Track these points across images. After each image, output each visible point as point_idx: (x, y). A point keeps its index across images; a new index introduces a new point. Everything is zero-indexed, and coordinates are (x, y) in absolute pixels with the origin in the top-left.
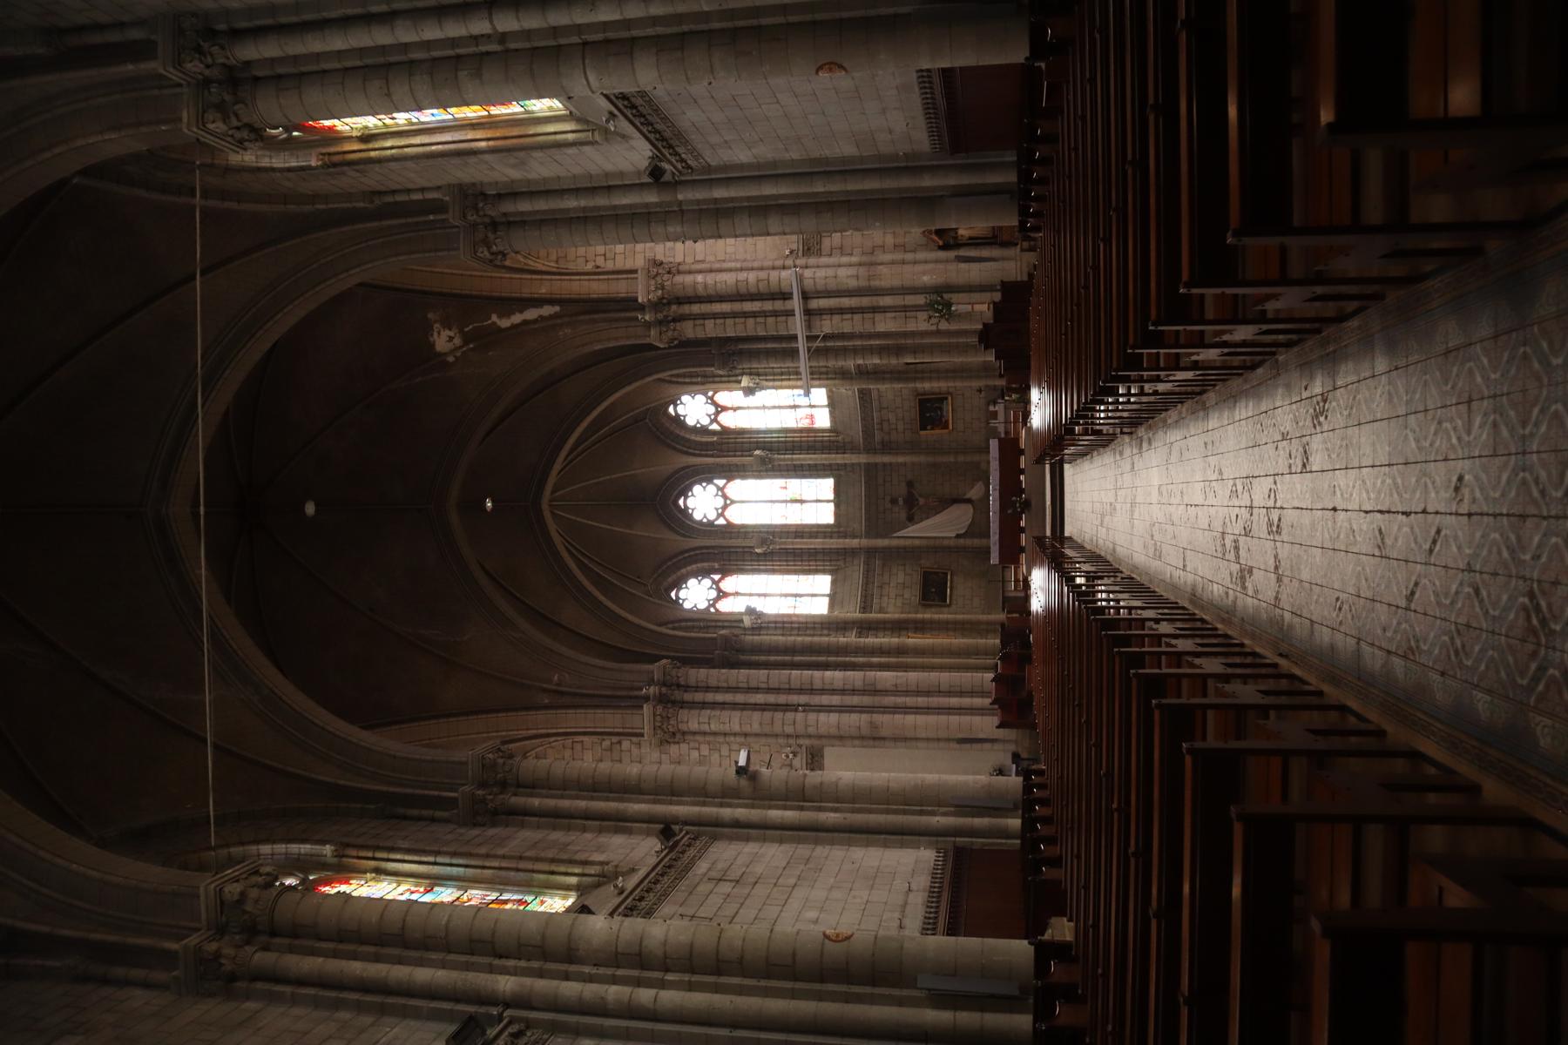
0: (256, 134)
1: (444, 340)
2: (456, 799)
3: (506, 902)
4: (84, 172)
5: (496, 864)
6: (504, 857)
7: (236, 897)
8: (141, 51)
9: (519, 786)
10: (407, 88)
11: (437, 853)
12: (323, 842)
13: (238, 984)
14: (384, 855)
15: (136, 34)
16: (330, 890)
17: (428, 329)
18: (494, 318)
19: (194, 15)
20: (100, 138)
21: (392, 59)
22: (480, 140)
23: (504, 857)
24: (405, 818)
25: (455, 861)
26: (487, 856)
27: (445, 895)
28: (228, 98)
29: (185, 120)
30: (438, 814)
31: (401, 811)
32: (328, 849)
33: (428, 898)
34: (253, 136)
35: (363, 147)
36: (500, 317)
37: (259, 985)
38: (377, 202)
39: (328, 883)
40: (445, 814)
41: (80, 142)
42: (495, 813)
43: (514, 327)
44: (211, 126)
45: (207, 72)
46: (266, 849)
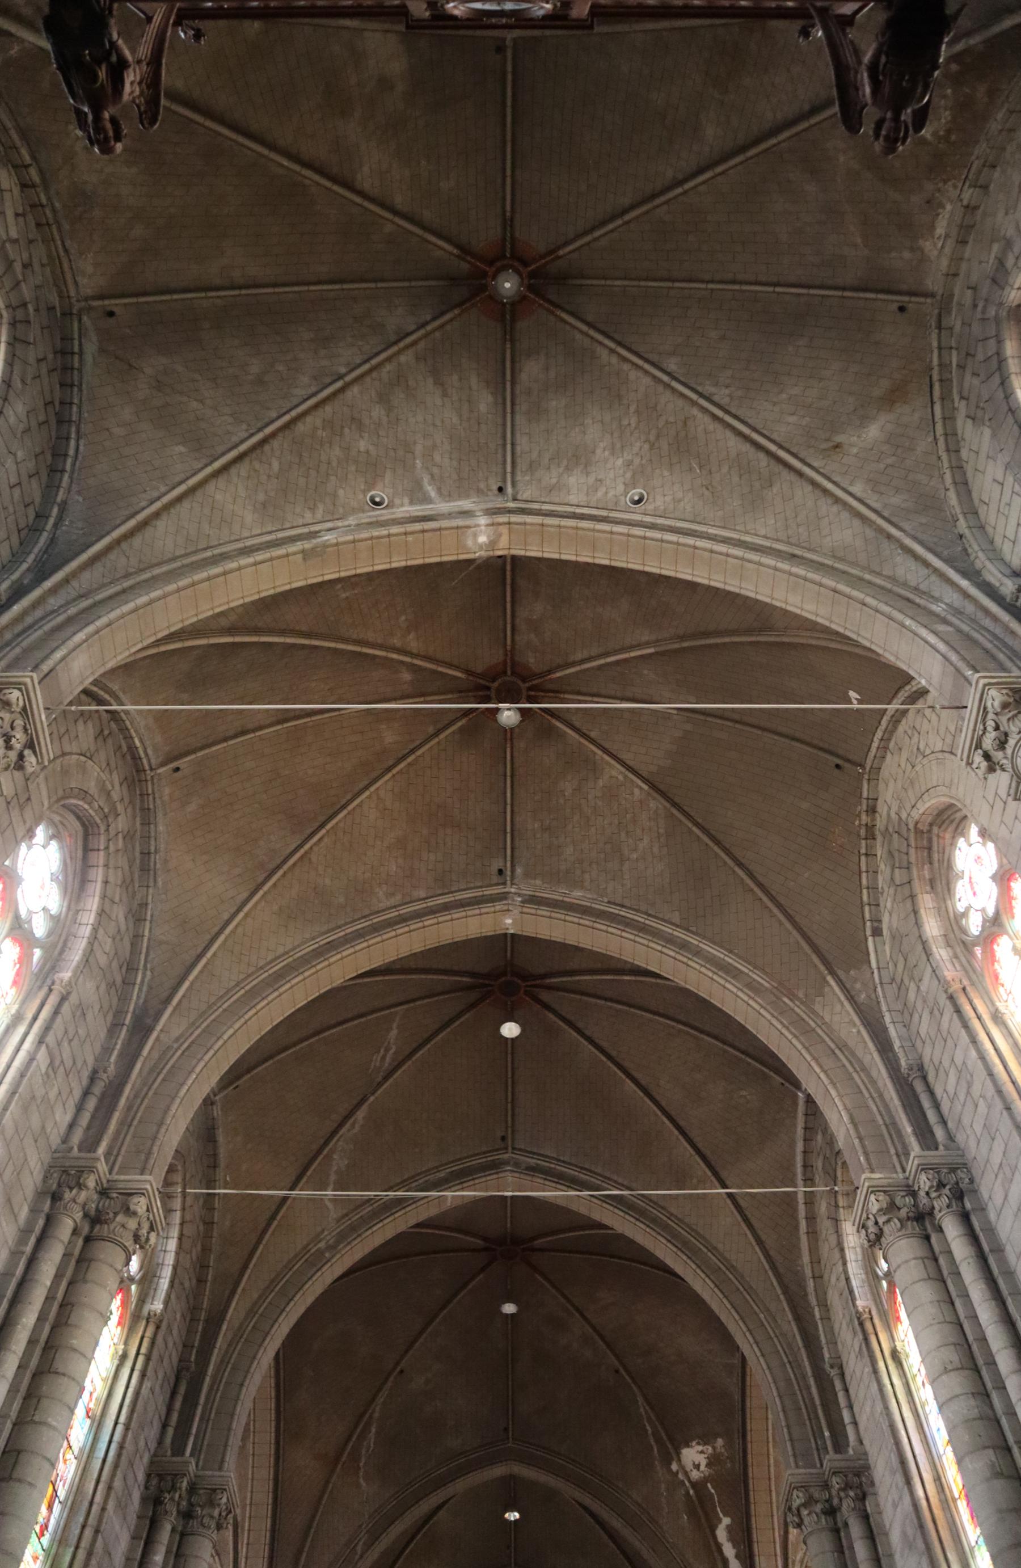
0: (876, 1241)
1: (694, 1457)
2: (183, 1454)
3: (50, 1507)
4: (810, 1100)
5: (98, 1498)
6: (103, 1509)
7: (132, 1207)
8: (925, 1136)
9: (183, 1535)
10: (958, 1390)
11: (127, 1427)
12: (167, 1302)
13: (48, 1202)
14: (139, 1366)
15: (939, 1133)
16: (116, 1304)
17: (706, 1439)
18: (726, 1521)
19: (972, 1181)
20: (841, 1108)
21: (984, 1372)
22: (925, 1489)
23: (103, 1509)
24: (174, 1393)
25: (114, 1446)
26: (110, 1488)
27: (79, 1431)
28: (903, 1213)
29: (873, 1176)
30: (170, 1431)
31: (182, 1389)
32: (158, 1306)
33: (80, 1411)
34: (872, 1237)
35: (887, 1353)
36: (729, 1528)
37: (41, 1222)
38: (833, 1372)
39: (124, 1304)
40: (168, 1440)
41: (833, 1093)
42: (158, 1502)
43: (719, 1547)
44: (873, 1198)
45: (922, 1193)
46: (172, 1245)
